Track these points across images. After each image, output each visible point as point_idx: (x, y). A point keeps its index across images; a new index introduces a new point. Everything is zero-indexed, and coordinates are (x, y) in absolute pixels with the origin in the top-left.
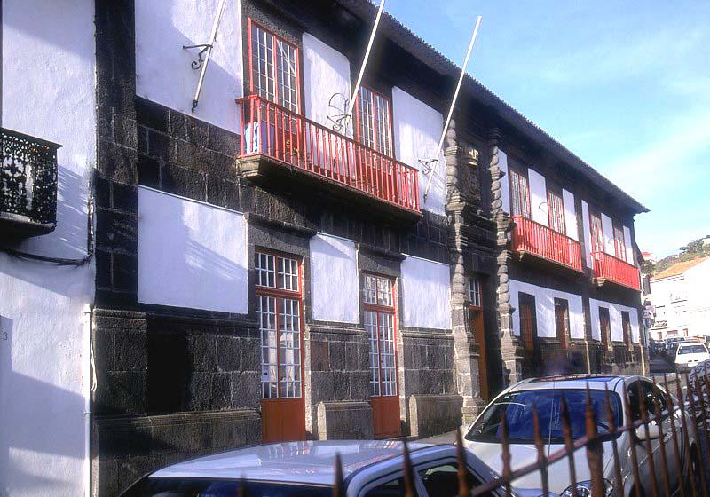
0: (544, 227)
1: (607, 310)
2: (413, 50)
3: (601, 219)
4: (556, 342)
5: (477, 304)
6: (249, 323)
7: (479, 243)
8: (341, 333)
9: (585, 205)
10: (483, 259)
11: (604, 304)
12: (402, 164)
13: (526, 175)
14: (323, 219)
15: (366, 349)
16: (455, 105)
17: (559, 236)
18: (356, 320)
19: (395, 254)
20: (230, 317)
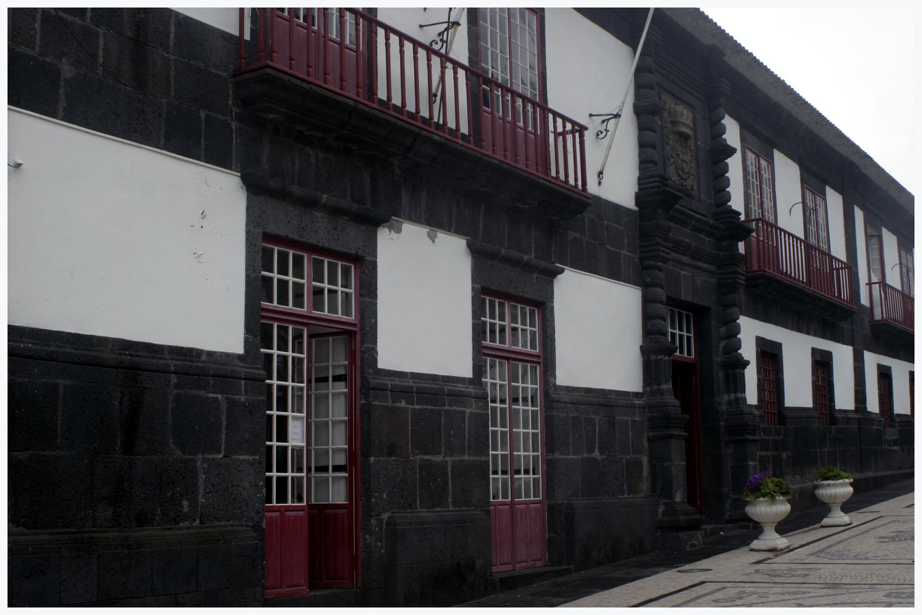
0: (797, 238)
1: (778, 346)
2: (758, 81)
3: (825, 199)
4: (242, 370)
5: (689, 353)
6: (471, 390)
7: (692, 257)
8: (430, 390)
9: (859, 215)
10: (699, 282)
11: (886, 361)
12: (556, 114)
13: (823, 195)
14: (405, 197)
15: (482, 422)
16: (644, 25)
17: (813, 250)
18: (465, 370)
19: (543, 264)
20: (204, 357)
